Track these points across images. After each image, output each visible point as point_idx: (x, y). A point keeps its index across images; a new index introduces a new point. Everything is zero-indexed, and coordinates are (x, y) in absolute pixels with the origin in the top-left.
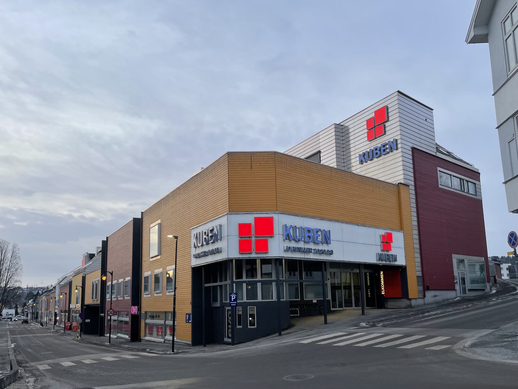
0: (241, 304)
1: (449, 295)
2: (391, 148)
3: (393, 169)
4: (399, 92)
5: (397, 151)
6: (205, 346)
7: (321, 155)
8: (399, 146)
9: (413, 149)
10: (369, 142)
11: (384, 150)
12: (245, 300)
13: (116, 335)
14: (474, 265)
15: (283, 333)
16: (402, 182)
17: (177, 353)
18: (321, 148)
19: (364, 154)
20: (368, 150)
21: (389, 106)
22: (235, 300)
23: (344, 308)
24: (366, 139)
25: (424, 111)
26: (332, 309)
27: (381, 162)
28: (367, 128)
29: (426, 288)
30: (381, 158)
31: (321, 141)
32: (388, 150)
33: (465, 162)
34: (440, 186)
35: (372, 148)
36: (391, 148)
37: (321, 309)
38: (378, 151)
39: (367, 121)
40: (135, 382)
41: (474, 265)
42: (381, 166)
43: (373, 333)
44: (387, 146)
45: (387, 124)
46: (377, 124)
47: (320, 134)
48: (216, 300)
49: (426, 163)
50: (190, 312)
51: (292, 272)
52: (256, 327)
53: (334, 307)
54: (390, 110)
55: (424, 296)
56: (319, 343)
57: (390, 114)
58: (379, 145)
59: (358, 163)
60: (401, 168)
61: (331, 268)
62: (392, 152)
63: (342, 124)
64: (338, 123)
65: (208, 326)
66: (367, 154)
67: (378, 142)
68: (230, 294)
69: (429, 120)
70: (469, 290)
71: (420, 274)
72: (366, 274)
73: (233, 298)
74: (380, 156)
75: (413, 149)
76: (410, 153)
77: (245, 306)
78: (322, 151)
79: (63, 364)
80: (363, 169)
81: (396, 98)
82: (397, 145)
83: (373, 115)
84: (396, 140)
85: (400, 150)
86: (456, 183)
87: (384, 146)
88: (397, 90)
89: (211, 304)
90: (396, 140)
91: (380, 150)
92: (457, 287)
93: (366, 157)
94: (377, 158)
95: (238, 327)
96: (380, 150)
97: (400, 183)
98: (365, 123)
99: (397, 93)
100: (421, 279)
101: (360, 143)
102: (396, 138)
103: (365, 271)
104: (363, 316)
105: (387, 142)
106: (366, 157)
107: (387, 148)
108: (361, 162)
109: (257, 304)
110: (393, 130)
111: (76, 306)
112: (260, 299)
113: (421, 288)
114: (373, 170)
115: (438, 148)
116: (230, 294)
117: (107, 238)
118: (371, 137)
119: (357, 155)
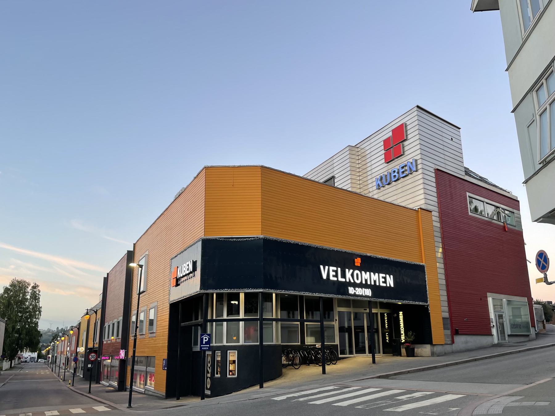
0: (218, 348)
1: (483, 340)
2: (411, 169)
3: (416, 194)
4: (418, 107)
5: (417, 173)
6: (178, 399)
7: (336, 180)
8: (420, 167)
9: (438, 172)
10: (387, 164)
11: (403, 172)
12: (225, 343)
13: (108, 382)
14: (520, 308)
15: (265, 385)
16: (423, 207)
17: (137, 409)
18: (335, 173)
19: (381, 178)
20: (386, 173)
21: (408, 123)
22: (206, 343)
23: (356, 355)
24: (383, 161)
25: (443, 125)
26: (340, 356)
27: (400, 186)
28: (384, 149)
29: (456, 333)
30: (399, 182)
31: (335, 165)
32: (407, 172)
33: (501, 189)
34: (470, 214)
35: (390, 171)
36: (411, 169)
37: (325, 356)
38: (396, 174)
39: (385, 141)
40: (427, 407)
41: (520, 308)
42: (400, 191)
43: (369, 388)
44: (406, 168)
45: (406, 143)
46: (395, 144)
47: (334, 157)
48: (196, 344)
49: (453, 187)
50: (166, 358)
51: (310, 312)
52: (236, 376)
53: (343, 352)
54: (408, 127)
55: (453, 342)
56: (276, 399)
57: (409, 132)
58: (398, 167)
59: (375, 188)
60: (422, 191)
61: (339, 306)
62: (411, 174)
63: (357, 146)
64: (354, 145)
65: (187, 374)
66: (384, 178)
67: (397, 164)
68: (202, 335)
69: (456, 140)
70: (509, 336)
71: (447, 315)
72: (382, 315)
73: (204, 341)
74: (398, 180)
75: (438, 172)
76: (433, 175)
77: (224, 350)
78: (336, 176)
79: (95, 408)
80: (381, 194)
81: (416, 113)
82: (417, 165)
83: (390, 134)
84: (416, 161)
85: (420, 171)
86: (490, 210)
87: (403, 168)
88: (416, 105)
89: (192, 348)
90: (416, 161)
91: (398, 173)
92: (494, 331)
93: (385, 181)
94: (395, 181)
95: (216, 376)
96: (398, 173)
97: (421, 208)
98: (382, 143)
99: (416, 109)
100: (449, 321)
101: (378, 166)
102: (415, 158)
103: (382, 311)
104: (373, 365)
105: (406, 162)
106: (385, 181)
107: (406, 170)
108: (379, 187)
109: (240, 349)
110: (412, 150)
111: (81, 349)
112: (242, 342)
113: (449, 332)
114: (393, 195)
115: (467, 172)
116: (202, 335)
117: (108, 274)
118: (388, 160)
119: (374, 179)
